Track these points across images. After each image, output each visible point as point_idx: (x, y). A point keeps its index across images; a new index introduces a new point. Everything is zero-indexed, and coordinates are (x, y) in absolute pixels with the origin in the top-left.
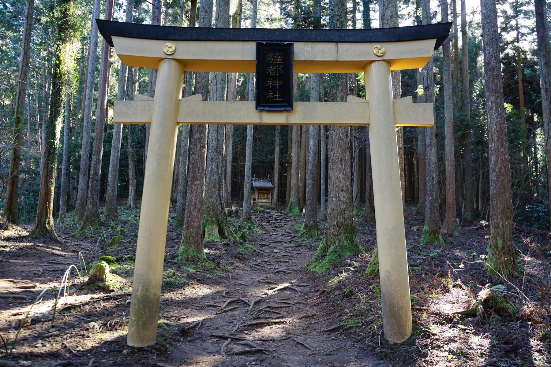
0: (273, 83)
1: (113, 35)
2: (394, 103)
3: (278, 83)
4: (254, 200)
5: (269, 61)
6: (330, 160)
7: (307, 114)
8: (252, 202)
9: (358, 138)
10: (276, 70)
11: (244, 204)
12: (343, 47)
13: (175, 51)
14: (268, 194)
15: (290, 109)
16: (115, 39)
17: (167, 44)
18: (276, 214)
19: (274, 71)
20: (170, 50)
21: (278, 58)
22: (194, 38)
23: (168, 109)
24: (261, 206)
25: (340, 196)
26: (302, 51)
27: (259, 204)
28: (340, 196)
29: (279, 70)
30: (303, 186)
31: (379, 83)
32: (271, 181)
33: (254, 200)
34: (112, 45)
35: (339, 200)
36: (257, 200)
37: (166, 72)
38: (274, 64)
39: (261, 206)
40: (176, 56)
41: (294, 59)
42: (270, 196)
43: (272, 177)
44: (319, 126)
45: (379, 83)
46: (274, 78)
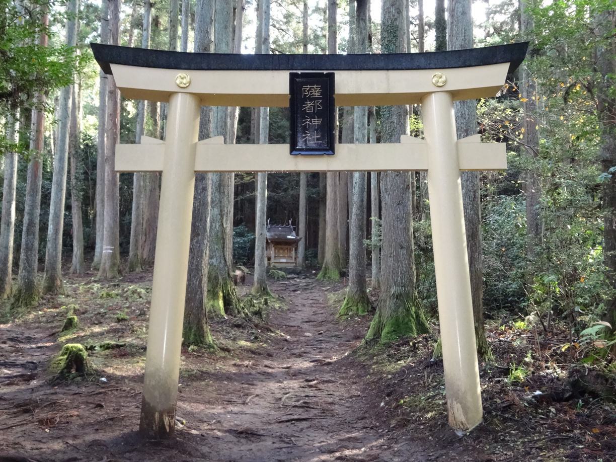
0: (311, 121)
1: (113, 63)
2: (457, 143)
3: (317, 122)
4: (269, 259)
5: (305, 95)
6: (383, 204)
7: (354, 157)
8: (266, 262)
9: (412, 186)
10: (314, 106)
11: (256, 266)
12: (395, 75)
13: (190, 83)
14: (290, 250)
15: (332, 153)
16: (114, 68)
17: (180, 74)
18: (304, 281)
19: (311, 104)
20: (185, 81)
21: (316, 91)
22: (212, 68)
23: (183, 154)
24: (281, 269)
25: (397, 254)
26: (347, 82)
27: (276, 265)
28: (397, 254)
29: (318, 106)
30: (345, 237)
31: (439, 116)
32: (294, 229)
33: (269, 259)
34: (111, 73)
35: (397, 261)
36: (272, 260)
37: (181, 110)
38: (311, 99)
39: (281, 269)
40: (190, 90)
41: (336, 92)
42: (293, 252)
43: (295, 223)
44: (369, 173)
45: (439, 116)
46: (312, 116)
